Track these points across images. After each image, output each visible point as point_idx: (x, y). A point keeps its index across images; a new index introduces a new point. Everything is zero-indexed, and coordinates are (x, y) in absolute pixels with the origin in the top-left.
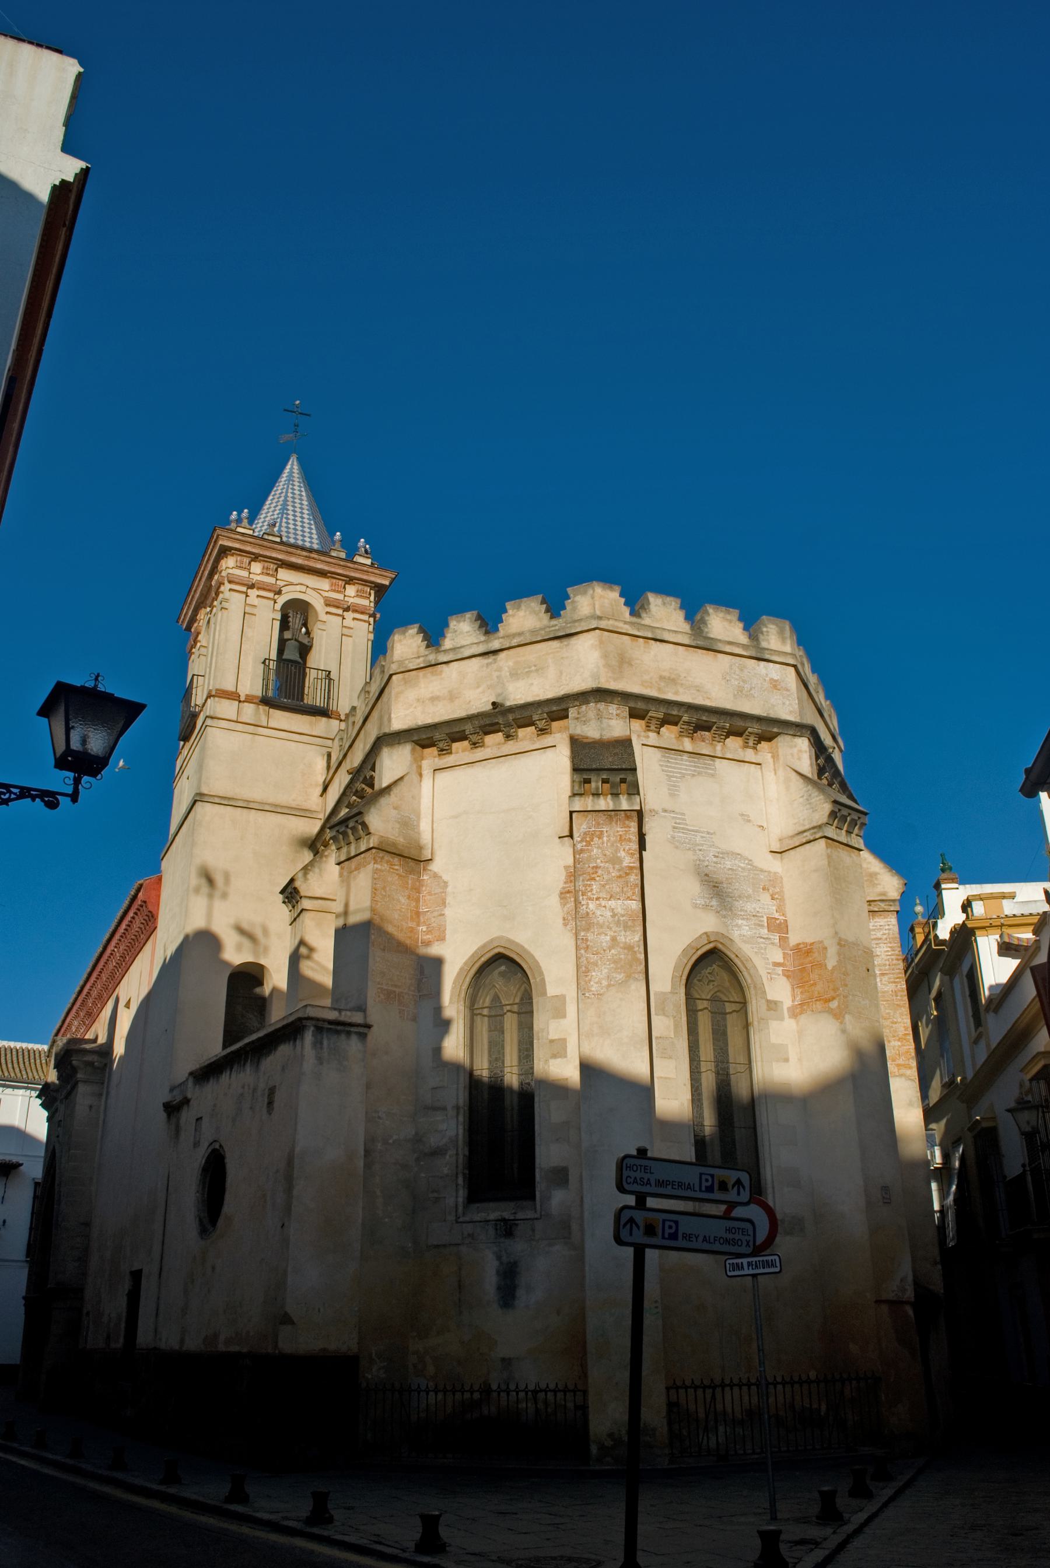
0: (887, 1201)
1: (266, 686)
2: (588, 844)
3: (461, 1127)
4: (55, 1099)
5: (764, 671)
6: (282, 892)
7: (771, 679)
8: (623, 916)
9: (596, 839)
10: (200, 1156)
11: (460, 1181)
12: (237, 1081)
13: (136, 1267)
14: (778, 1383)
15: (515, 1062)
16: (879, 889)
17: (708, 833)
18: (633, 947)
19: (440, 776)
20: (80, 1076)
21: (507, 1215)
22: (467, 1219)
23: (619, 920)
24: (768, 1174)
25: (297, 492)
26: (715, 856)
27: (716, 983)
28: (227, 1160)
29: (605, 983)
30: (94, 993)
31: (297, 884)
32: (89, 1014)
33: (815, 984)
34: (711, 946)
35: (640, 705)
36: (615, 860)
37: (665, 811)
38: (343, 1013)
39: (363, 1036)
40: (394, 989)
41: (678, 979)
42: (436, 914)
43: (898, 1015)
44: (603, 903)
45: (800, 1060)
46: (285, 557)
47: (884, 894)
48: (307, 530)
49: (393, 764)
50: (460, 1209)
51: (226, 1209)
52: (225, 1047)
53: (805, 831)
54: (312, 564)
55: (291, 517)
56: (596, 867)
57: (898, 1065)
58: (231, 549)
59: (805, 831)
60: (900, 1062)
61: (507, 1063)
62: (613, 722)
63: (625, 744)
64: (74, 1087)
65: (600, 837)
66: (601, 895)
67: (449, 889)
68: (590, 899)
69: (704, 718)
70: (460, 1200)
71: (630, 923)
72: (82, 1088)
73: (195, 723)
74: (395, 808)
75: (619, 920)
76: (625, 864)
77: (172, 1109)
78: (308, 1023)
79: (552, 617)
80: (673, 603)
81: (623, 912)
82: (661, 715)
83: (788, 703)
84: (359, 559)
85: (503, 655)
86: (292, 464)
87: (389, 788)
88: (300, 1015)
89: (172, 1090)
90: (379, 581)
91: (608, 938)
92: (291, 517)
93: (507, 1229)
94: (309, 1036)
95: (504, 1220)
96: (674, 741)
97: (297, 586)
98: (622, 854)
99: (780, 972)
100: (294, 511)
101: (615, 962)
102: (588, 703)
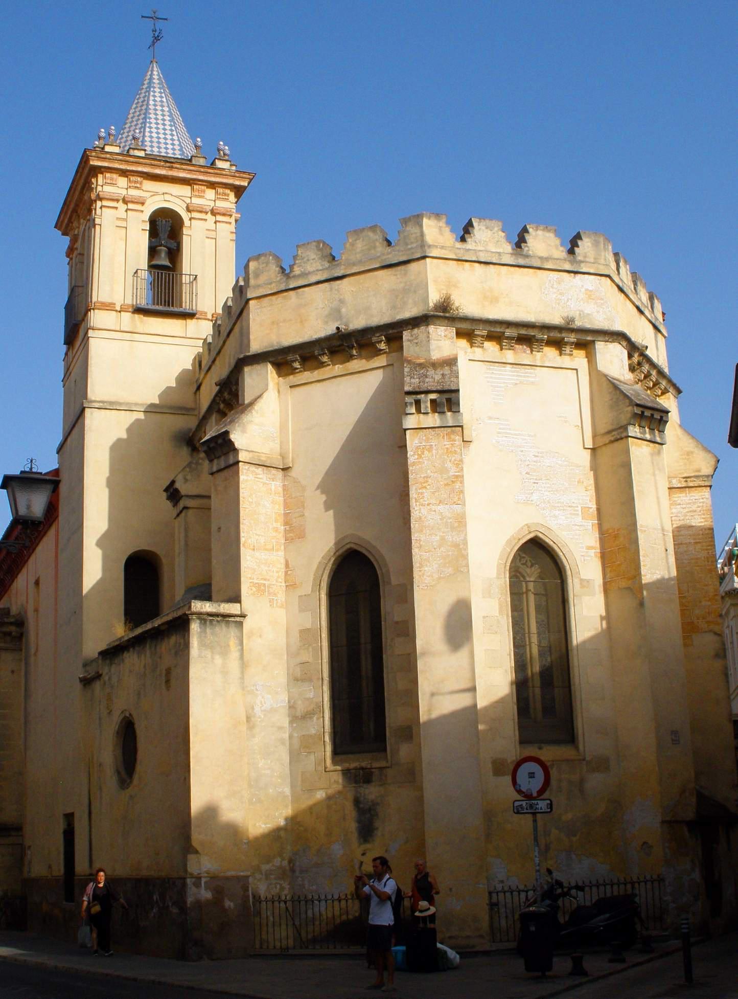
0: (675, 742)
2: (420, 456)
6: (166, 490)
7: (587, 290)
9: (426, 452)
10: (116, 718)
12: (132, 661)
13: (69, 811)
17: (529, 436)
21: (364, 764)
24: (579, 724)
25: (158, 99)
28: (136, 726)
29: (436, 576)
31: (177, 485)
36: (443, 470)
37: (490, 418)
39: (240, 624)
41: (503, 566)
44: (433, 508)
47: (699, 471)
48: (169, 137)
51: (138, 768)
55: (154, 126)
56: (427, 477)
57: (708, 622)
61: (362, 640)
63: (451, 362)
65: (430, 450)
68: (422, 505)
71: (456, 525)
76: (451, 474)
77: (87, 682)
80: (497, 226)
82: (485, 333)
84: (220, 164)
85: (345, 281)
89: (85, 665)
92: (154, 126)
95: (362, 768)
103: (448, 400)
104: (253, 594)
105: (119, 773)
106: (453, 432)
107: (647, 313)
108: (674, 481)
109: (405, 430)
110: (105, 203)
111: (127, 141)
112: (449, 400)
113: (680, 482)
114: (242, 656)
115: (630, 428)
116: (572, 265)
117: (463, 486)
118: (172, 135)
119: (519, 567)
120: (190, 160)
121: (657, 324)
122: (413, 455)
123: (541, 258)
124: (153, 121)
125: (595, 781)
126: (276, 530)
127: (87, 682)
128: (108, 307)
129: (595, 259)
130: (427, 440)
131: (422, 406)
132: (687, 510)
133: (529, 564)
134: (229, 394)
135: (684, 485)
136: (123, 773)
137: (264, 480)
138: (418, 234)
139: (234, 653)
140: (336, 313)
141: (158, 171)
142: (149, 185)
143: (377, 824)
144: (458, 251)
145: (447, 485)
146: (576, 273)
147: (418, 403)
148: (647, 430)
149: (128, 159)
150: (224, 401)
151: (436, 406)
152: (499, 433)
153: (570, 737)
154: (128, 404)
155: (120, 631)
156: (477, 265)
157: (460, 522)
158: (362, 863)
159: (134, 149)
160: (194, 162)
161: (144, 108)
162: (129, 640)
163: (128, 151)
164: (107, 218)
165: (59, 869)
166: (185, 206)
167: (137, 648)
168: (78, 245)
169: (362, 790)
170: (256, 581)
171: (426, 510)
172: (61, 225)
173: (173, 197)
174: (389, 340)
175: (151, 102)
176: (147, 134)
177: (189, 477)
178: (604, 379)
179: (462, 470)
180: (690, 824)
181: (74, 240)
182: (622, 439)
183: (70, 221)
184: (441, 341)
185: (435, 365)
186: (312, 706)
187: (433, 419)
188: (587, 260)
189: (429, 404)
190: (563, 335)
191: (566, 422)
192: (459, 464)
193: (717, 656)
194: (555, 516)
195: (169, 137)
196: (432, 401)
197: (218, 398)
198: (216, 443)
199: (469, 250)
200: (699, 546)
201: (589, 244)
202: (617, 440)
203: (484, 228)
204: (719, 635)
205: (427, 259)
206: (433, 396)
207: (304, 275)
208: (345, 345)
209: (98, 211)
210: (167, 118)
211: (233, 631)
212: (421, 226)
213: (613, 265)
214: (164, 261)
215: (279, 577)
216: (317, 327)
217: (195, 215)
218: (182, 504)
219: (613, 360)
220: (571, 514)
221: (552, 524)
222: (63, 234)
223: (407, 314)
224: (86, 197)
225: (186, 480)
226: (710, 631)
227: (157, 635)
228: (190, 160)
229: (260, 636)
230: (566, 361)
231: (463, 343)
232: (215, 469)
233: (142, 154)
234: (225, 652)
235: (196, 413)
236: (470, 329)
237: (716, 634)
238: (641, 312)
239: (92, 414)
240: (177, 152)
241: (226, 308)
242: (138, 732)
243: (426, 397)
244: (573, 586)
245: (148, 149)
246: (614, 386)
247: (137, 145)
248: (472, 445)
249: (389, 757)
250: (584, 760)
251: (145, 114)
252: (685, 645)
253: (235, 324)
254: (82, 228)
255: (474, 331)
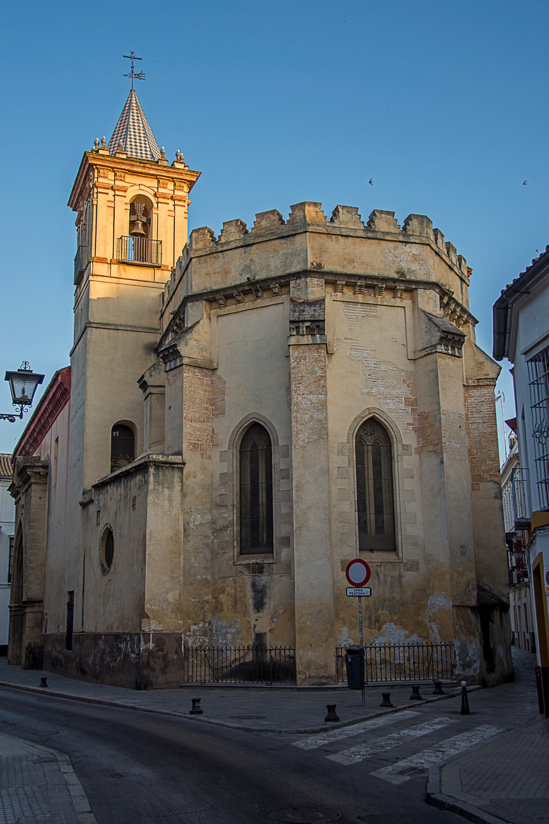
0: (463, 554)
2: (298, 363)
3: (235, 516)
4: (18, 493)
5: (409, 250)
6: (138, 382)
7: (413, 254)
8: (317, 404)
10: (101, 529)
11: (235, 544)
12: (114, 493)
14: (434, 646)
15: (264, 481)
16: (485, 372)
17: (371, 350)
18: (322, 421)
19: (220, 319)
20: (32, 480)
22: (238, 563)
23: (314, 406)
24: (399, 538)
25: (136, 118)
26: (375, 364)
27: (375, 435)
28: (114, 534)
30: (37, 430)
32: (35, 440)
33: (429, 436)
34: (371, 415)
35: (330, 278)
36: (313, 372)
37: (346, 339)
38: (170, 457)
39: (181, 470)
40: (197, 442)
42: (220, 399)
43: (491, 446)
44: (306, 396)
45: (421, 477)
47: (487, 375)
49: (195, 312)
50: (236, 558)
51: (114, 561)
52: (112, 471)
53: (427, 348)
54: (146, 171)
55: (133, 137)
56: (302, 376)
57: (490, 475)
59: (427, 348)
60: (492, 473)
61: (260, 481)
62: (315, 289)
63: (321, 302)
64: (29, 487)
66: (305, 392)
67: (227, 385)
68: (299, 394)
69: (370, 283)
70: (236, 554)
71: (320, 408)
72: (34, 487)
73: (83, 276)
74: (195, 341)
75: (314, 406)
76: (318, 375)
77: (84, 505)
78: (151, 464)
81: (316, 402)
82: (344, 283)
83: (422, 268)
84: (177, 165)
87: (192, 327)
88: (146, 459)
91: (308, 416)
92: (133, 137)
93: (258, 569)
94: (152, 470)
95: (257, 563)
96: (352, 296)
98: (317, 369)
99: (411, 429)
101: (312, 429)
102: (300, 278)
103: (317, 326)
104: (191, 450)
105: (102, 565)
106: (320, 348)
107: (456, 269)
108: (470, 381)
109: (289, 346)
110: (99, 190)
111: (114, 147)
112: (318, 327)
113: (474, 382)
114: (182, 490)
115: (439, 346)
116: (404, 237)
117: (326, 383)
118: (145, 144)
119: (362, 436)
120: (157, 162)
121: (463, 277)
122: (294, 362)
123: (383, 233)
124: (132, 133)
125: (409, 577)
126: (206, 409)
127: (84, 505)
128: (103, 261)
129: (420, 233)
130: (304, 352)
131: (301, 330)
132: (478, 400)
133: (369, 434)
134: (179, 320)
135: (477, 384)
136: (105, 565)
137: (199, 377)
138: (302, 217)
139: (178, 488)
140: (247, 268)
141: (135, 169)
142: (129, 178)
143: (266, 600)
144: (328, 228)
145: (315, 382)
146: (407, 243)
147: (298, 328)
148: (450, 348)
149: (115, 160)
150: (176, 325)
151: (311, 331)
152: (351, 348)
153: (394, 548)
154: (114, 325)
155: (106, 473)
156: (340, 237)
157: (324, 405)
158: (255, 626)
159: (119, 153)
160: (160, 164)
161: (126, 124)
162: (110, 478)
163: (115, 155)
164: (102, 200)
165: (63, 629)
166: (153, 193)
167: (116, 484)
168: (83, 218)
169: (257, 578)
170: (192, 441)
171: (303, 399)
172: (72, 204)
173: (145, 187)
174: (282, 286)
175: (131, 120)
176: (128, 143)
177: (153, 374)
178: (422, 314)
179: (325, 372)
180: (472, 608)
181: (81, 215)
182: (432, 353)
183: (78, 201)
184: (315, 289)
185: (310, 304)
186: (227, 522)
187: (307, 339)
188: (415, 234)
189: (305, 329)
190: (396, 285)
191: (396, 342)
192: (323, 369)
193: (496, 497)
194: (386, 403)
195: (143, 145)
196: (307, 327)
197: (172, 323)
198: (169, 352)
199: (335, 227)
200: (485, 425)
201: (417, 223)
202: (429, 354)
203: (345, 212)
204: (498, 484)
205: (307, 234)
206: (308, 324)
207: (227, 243)
208: (254, 288)
209: (95, 195)
210: (142, 132)
211: (177, 474)
212: (304, 211)
213: (432, 237)
214: (140, 229)
215: (207, 439)
216: (236, 278)
217: (161, 200)
218: (148, 392)
219: (429, 301)
220: (397, 402)
221: (385, 408)
222: (73, 210)
223: (293, 270)
224: (87, 186)
225: (151, 376)
226: (492, 481)
227: (128, 474)
228: (157, 162)
229: (194, 477)
230: (398, 302)
231: (330, 289)
232: (168, 369)
233: (124, 157)
234: (171, 488)
235: (160, 332)
236: (333, 280)
237: (495, 482)
238: (452, 269)
239: (91, 331)
240: (149, 156)
241: (179, 262)
242: (114, 539)
243: (303, 324)
244: (397, 449)
245: (129, 153)
246: (429, 317)
247: (121, 150)
248: (333, 357)
249: (275, 557)
250: (402, 562)
251: (127, 128)
252: (474, 489)
253: (183, 274)
254: (85, 206)
255: (336, 281)
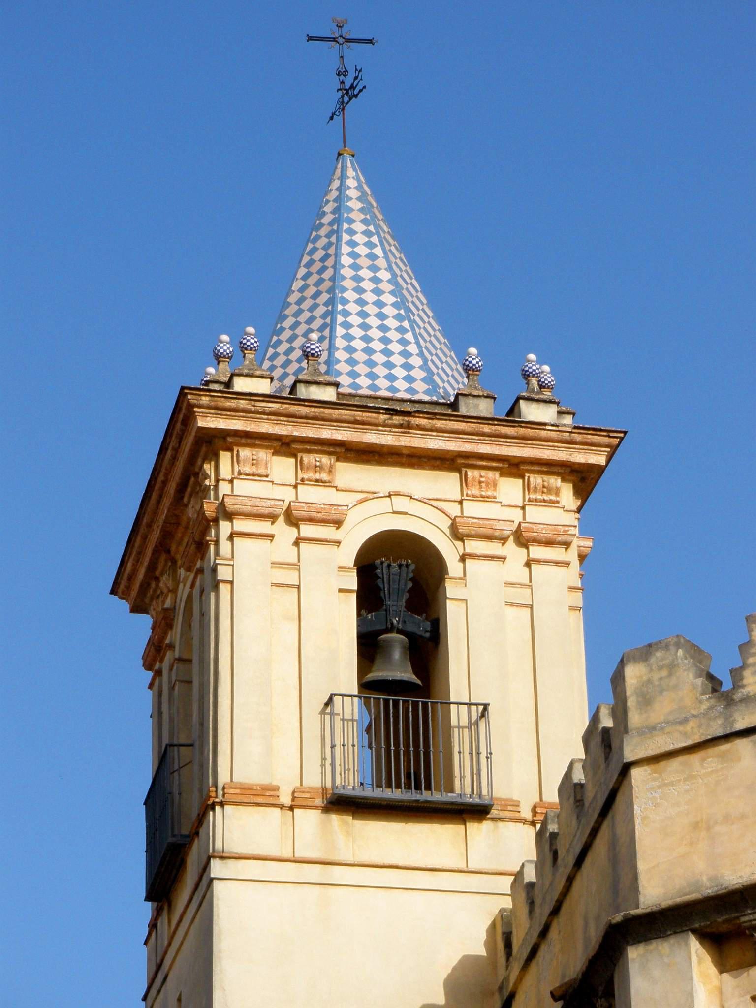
1: (329, 762)
25: (362, 250)
46: (384, 432)
58: (224, 434)
79: (552, 994)
86: (343, 177)
90: (580, 457)
97: (414, 503)
100: (361, 302)
